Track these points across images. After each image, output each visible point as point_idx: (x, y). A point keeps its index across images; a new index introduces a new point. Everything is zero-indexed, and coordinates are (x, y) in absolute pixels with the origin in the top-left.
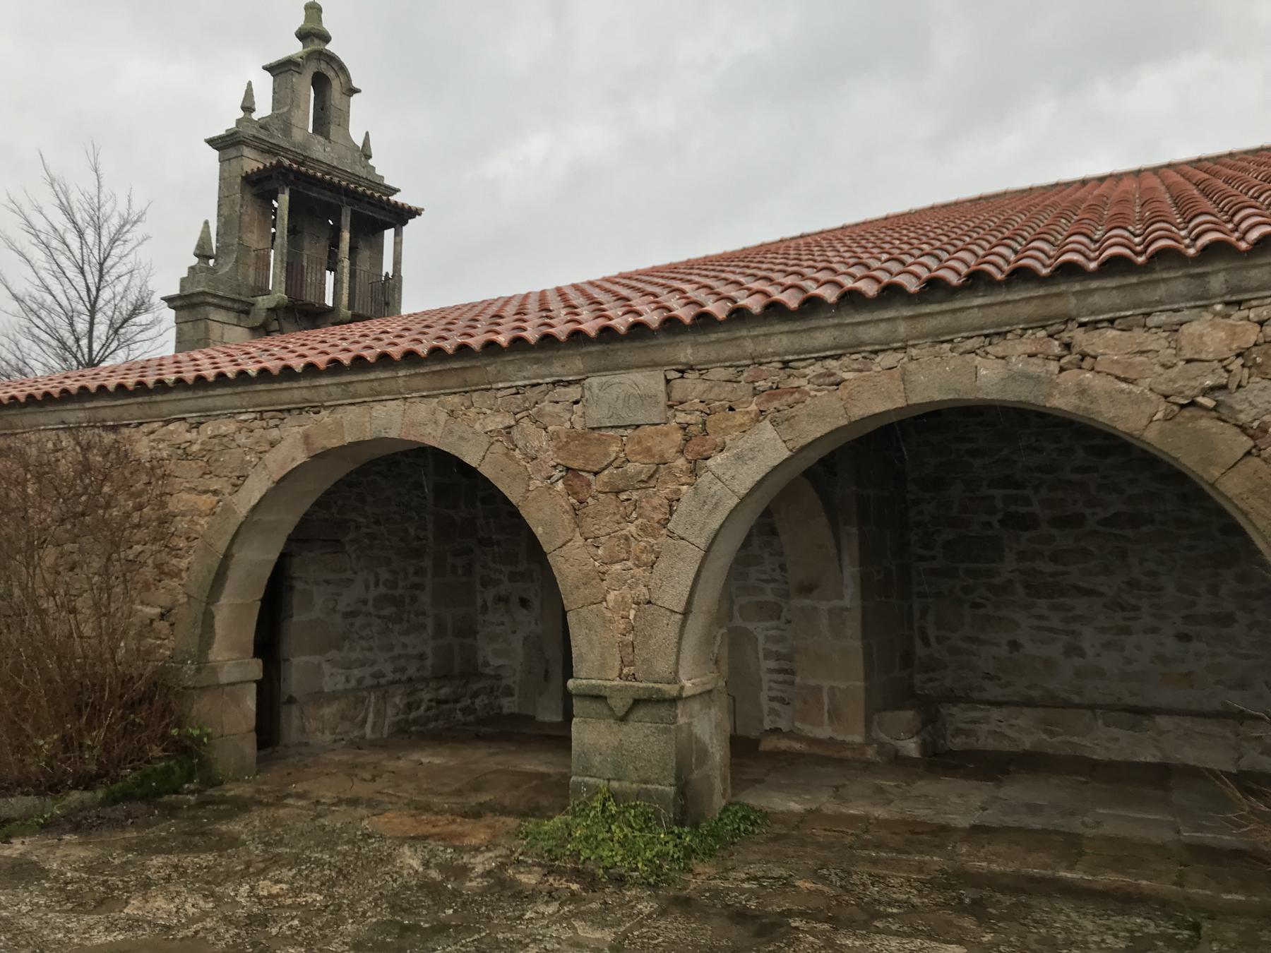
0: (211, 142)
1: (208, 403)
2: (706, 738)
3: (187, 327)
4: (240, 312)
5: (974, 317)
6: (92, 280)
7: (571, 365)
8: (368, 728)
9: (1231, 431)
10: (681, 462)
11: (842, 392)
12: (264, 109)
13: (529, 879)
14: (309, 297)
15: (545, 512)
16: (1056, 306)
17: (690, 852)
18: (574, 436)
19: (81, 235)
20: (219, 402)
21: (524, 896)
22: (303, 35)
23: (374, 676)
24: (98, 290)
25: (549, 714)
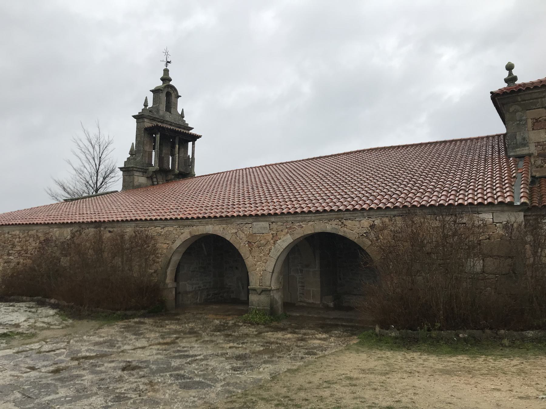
0: (134, 117)
1: (166, 223)
2: (277, 299)
3: (127, 177)
4: (143, 172)
5: (326, 217)
6: (97, 163)
7: (251, 220)
8: (198, 300)
9: (368, 241)
10: (272, 241)
11: (303, 229)
12: (150, 104)
13: (240, 324)
14: (165, 166)
15: (244, 251)
16: (339, 216)
17: (272, 320)
18: (250, 235)
19: (94, 148)
20: (169, 223)
21: (239, 326)
22: (162, 79)
23: (198, 287)
24: (99, 166)
25: (244, 298)
